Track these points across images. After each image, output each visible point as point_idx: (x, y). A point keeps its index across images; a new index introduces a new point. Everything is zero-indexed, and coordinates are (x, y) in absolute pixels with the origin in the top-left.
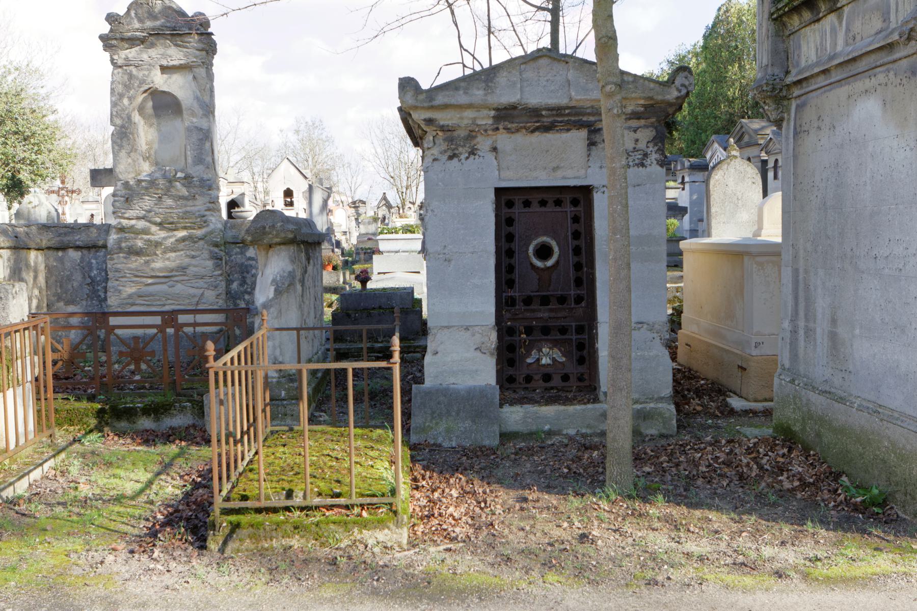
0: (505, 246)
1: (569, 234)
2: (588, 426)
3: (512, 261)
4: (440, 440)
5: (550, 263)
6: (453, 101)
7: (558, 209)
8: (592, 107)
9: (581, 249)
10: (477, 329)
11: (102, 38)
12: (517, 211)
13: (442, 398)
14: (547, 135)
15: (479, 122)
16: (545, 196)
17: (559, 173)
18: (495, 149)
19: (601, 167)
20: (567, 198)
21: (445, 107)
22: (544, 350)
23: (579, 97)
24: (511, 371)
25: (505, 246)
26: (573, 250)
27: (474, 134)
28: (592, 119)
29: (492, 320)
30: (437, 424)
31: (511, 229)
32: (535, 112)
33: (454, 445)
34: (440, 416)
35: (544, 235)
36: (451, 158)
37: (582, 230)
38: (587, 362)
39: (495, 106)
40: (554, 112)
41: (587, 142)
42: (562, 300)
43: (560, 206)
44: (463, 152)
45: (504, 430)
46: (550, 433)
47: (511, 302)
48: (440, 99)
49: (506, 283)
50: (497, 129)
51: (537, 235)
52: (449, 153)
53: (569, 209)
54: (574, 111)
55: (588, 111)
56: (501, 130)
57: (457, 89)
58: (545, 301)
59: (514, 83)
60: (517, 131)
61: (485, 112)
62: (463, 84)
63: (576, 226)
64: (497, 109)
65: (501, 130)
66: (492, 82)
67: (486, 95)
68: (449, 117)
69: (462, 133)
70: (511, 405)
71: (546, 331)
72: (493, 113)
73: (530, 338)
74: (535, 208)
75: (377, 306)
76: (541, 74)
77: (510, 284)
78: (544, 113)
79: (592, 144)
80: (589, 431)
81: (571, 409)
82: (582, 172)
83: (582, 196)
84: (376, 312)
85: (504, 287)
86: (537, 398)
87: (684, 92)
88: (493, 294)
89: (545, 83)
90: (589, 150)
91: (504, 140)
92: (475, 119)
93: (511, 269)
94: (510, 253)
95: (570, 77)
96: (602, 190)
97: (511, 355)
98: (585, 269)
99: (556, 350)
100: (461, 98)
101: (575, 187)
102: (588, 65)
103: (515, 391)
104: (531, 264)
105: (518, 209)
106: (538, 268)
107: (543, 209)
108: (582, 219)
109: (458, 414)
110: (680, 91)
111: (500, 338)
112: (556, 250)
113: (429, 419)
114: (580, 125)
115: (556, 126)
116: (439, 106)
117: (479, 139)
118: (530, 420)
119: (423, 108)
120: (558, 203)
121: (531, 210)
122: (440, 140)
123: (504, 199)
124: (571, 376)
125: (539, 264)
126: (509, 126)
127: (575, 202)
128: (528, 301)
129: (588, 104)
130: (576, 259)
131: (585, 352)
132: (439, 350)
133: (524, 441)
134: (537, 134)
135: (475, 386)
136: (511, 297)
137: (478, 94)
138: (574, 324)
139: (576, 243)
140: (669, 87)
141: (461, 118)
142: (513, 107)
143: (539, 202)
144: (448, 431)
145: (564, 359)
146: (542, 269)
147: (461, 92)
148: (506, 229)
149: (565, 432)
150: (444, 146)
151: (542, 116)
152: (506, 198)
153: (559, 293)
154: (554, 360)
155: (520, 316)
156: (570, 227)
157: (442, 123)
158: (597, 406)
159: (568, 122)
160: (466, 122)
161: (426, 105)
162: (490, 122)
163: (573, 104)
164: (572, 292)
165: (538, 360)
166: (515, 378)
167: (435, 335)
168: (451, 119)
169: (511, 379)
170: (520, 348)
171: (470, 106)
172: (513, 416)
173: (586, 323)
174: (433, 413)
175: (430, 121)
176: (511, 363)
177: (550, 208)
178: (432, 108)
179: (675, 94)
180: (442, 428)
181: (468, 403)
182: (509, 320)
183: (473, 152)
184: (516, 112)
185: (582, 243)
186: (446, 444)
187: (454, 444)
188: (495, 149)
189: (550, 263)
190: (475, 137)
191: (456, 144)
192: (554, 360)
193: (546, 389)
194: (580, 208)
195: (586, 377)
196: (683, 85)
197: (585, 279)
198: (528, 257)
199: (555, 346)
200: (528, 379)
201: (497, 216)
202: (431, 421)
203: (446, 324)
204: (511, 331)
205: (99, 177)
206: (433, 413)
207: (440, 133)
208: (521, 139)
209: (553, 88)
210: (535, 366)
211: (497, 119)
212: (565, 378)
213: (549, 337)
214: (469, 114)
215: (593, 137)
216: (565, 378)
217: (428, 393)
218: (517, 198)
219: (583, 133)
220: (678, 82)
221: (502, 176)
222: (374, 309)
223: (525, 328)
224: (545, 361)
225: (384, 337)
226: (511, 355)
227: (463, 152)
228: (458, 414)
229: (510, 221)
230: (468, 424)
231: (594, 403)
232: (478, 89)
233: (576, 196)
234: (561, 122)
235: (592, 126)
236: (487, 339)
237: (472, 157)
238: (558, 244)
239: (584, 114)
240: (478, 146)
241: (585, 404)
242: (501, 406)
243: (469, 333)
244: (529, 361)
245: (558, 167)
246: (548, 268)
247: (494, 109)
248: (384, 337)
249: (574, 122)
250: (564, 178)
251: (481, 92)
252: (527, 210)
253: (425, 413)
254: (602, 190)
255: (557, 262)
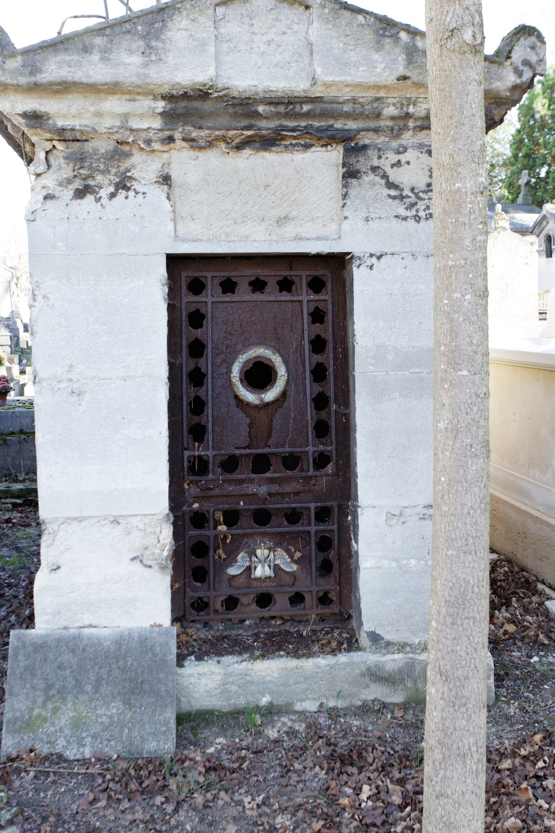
0: (187, 364)
1: (306, 343)
2: (339, 695)
3: (201, 393)
5: (270, 395)
6: (79, 76)
7: (285, 296)
8: (354, 101)
9: (325, 370)
10: (134, 521)
12: (210, 300)
13: (66, 657)
14: (267, 155)
15: (135, 124)
16: (262, 272)
17: (290, 230)
18: (166, 180)
19: (367, 220)
20: (302, 275)
21: (64, 88)
22: (259, 552)
23: (329, 79)
24: (198, 591)
25: (187, 364)
27: (126, 148)
28: (352, 125)
29: (163, 504)
30: (55, 710)
31: (198, 333)
32: (243, 107)
33: (87, 755)
34: (63, 693)
35: (260, 343)
36: (80, 194)
37: (329, 336)
38: (335, 572)
39: (165, 90)
40: (281, 109)
41: (342, 171)
42: (291, 462)
43: (289, 291)
44: (105, 183)
45: (185, 707)
46: (270, 712)
47: (200, 467)
48: (54, 70)
49: (190, 432)
50: (171, 139)
51: (247, 345)
52: (78, 184)
53: (306, 296)
54: (318, 107)
55: (346, 108)
56: (179, 143)
57: (86, 50)
58: (261, 464)
59: (204, 44)
60: (210, 144)
61: (146, 103)
62: (98, 41)
63: (317, 328)
64: (169, 98)
65: (179, 143)
66: (157, 38)
67: (145, 65)
68: (73, 111)
69: (103, 146)
70: (199, 658)
71: (262, 517)
72: (161, 105)
73: (234, 532)
74: (244, 293)
75: (17, 429)
76: (256, 29)
77: (198, 433)
78: (261, 109)
79: (351, 174)
80: (340, 704)
81: (309, 664)
82: (333, 227)
83: (329, 273)
84: (13, 438)
85: (187, 438)
86: (244, 634)
87: (527, 75)
88: (165, 456)
89: (264, 48)
90: (345, 186)
91: (184, 162)
92: (126, 117)
93: (198, 406)
94: (197, 378)
95: (312, 38)
96: (369, 262)
97: (199, 562)
98: (334, 407)
99: (280, 552)
100: (94, 70)
101: (318, 257)
102: (347, 14)
103: (206, 624)
104: (236, 397)
105: (211, 296)
106: (248, 404)
107: (258, 296)
108: (330, 316)
109: (96, 689)
110: (519, 74)
111: (177, 536)
112: (282, 371)
113: (40, 700)
114: (329, 138)
115: (284, 138)
116: (51, 84)
117: (137, 158)
118: (234, 688)
119: (18, 88)
120: (286, 285)
121: (235, 298)
122: (57, 160)
123: (186, 275)
124: (307, 596)
125: (249, 396)
126: (194, 135)
127: (316, 285)
128: (230, 464)
129: (347, 94)
130: (318, 388)
131: (332, 554)
132: (61, 562)
133: (223, 732)
134: (247, 152)
136: (200, 457)
137: (128, 63)
138: (312, 506)
139: (318, 358)
140: (500, 64)
141: (99, 114)
142: (202, 94)
143: (251, 284)
144: (77, 724)
145: (295, 567)
146: (256, 406)
147: (95, 57)
148: (188, 334)
149: (298, 707)
150: (67, 172)
151: (257, 115)
152: (190, 276)
153: (287, 449)
154: (277, 569)
155: (217, 492)
156: (308, 330)
157: (60, 123)
158: (356, 656)
159: (307, 131)
160: (108, 122)
161: (23, 80)
162: (157, 123)
163: (317, 92)
164: (310, 449)
165: (249, 570)
166: (205, 601)
167: (55, 533)
168: (79, 115)
169: (201, 605)
170: (216, 548)
171: (113, 88)
172: (203, 681)
173: (334, 504)
174: (49, 687)
175: (35, 118)
176: (200, 575)
177: (271, 294)
178: (35, 88)
179: (511, 79)
180: (64, 718)
181: (116, 666)
182: (197, 499)
183: (123, 184)
184: (207, 106)
185: (328, 358)
186: (70, 754)
187: (87, 752)
188: (166, 180)
189: (270, 395)
190: (128, 155)
191: (90, 168)
192: (277, 569)
193: (262, 619)
194: (326, 296)
195: (333, 596)
196: (526, 63)
197: (333, 425)
198: (230, 384)
199: (279, 544)
200: (231, 603)
201: (171, 308)
202: (44, 703)
203: (76, 515)
204: (199, 520)
206: (49, 687)
207: (60, 146)
208: (216, 160)
209: (279, 58)
211: (170, 117)
212: (297, 599)
214: (114, 105)
215: (353, 160)
216: (297, 599)
217: (41, 647)
218: (209, 275)
219: (335, 154)
220: (517, 55)
221: (180, 233)
222: (12, 433)
223: (226, 514)
224: (261, 571)
225: (27, 474)
226: (199, 562)
227: (105, 183)
228: (96, 689)
229: (197, 319)
230: (115, 708)
231: (349, 650)
232: (131, 52)
233: (320, 272)
234: (293, 130)
235: (350, 139)
236: (153, 540)
237: (122, 193)
238: (286, 361)
239: (338, 115)
240: (134, 173)
241: (333, 652)
242: (181, 660)
243: (119, 529)
244: (232, 571)
245: (286, 217)
246: (268, 405)
247: (164, 98)
248: (27, 474)
249: (319, 130)
250: (299, 238)
251: (136, 59)
252: (228, 297)
254: (369, 262)
255: (284, 394)
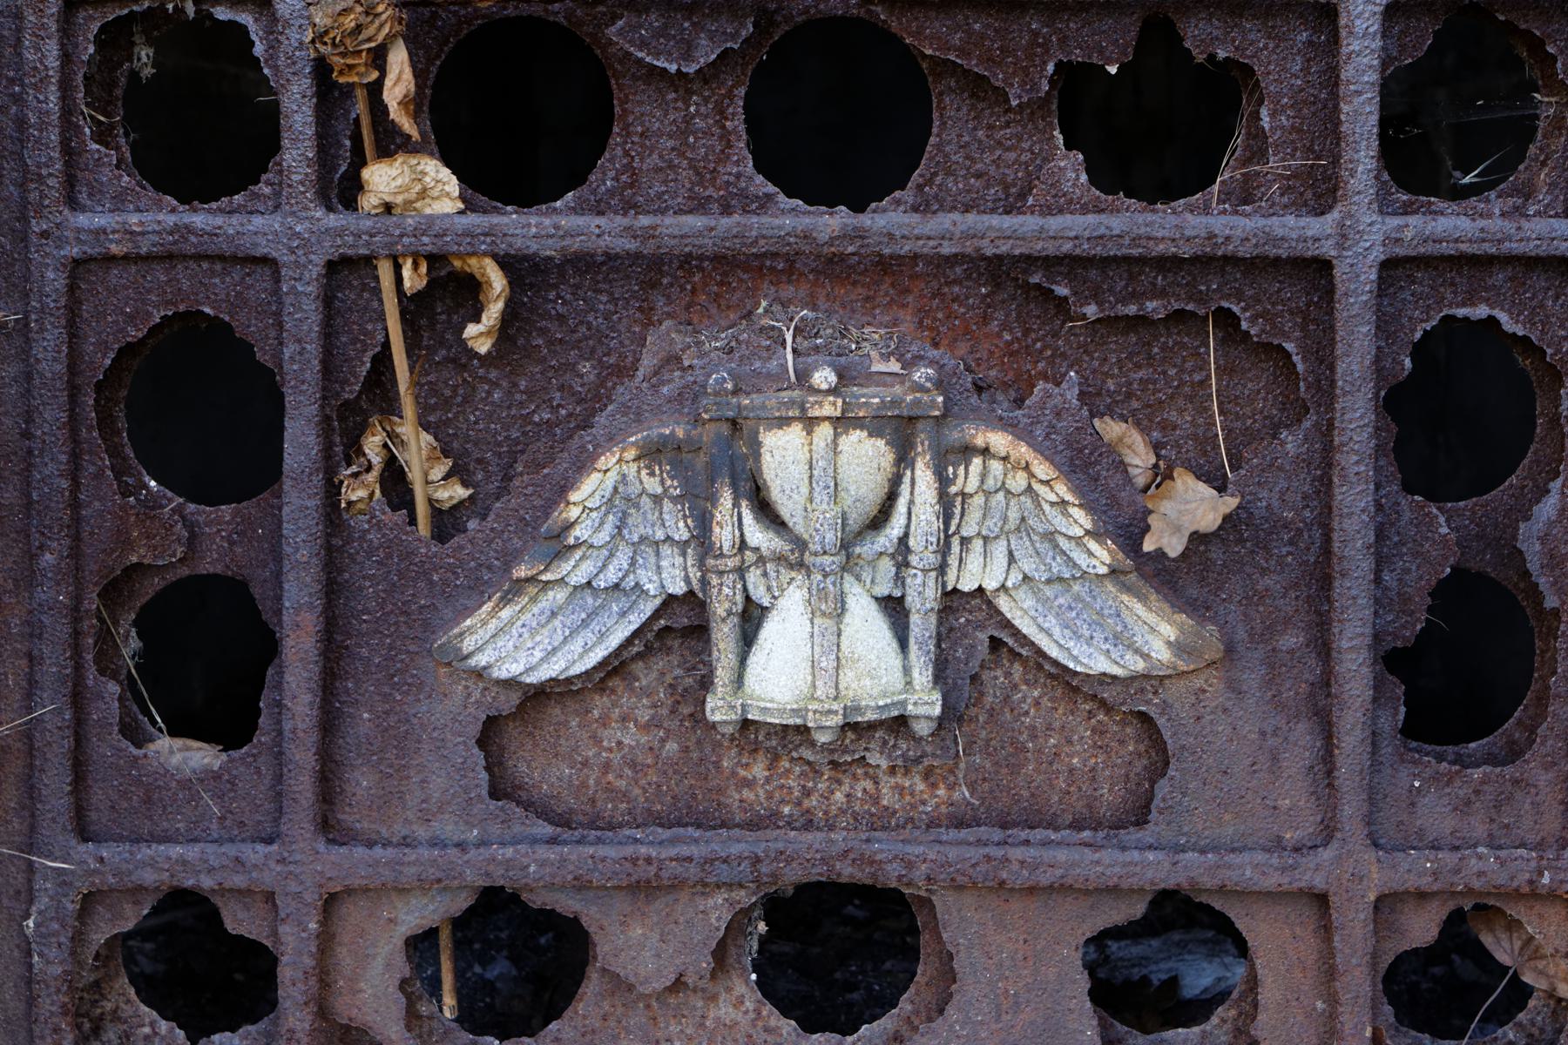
22: (784, 455)
26: (1396, 402)
73: (537, 228)
99: (1008, 465)
154: (969, 638)
170: (359, 404)
192: (969, 638)
199: (1001, 389)
210: (626, 731)
213: (891, 221)
224: (812, 658)
244: (520, 641)
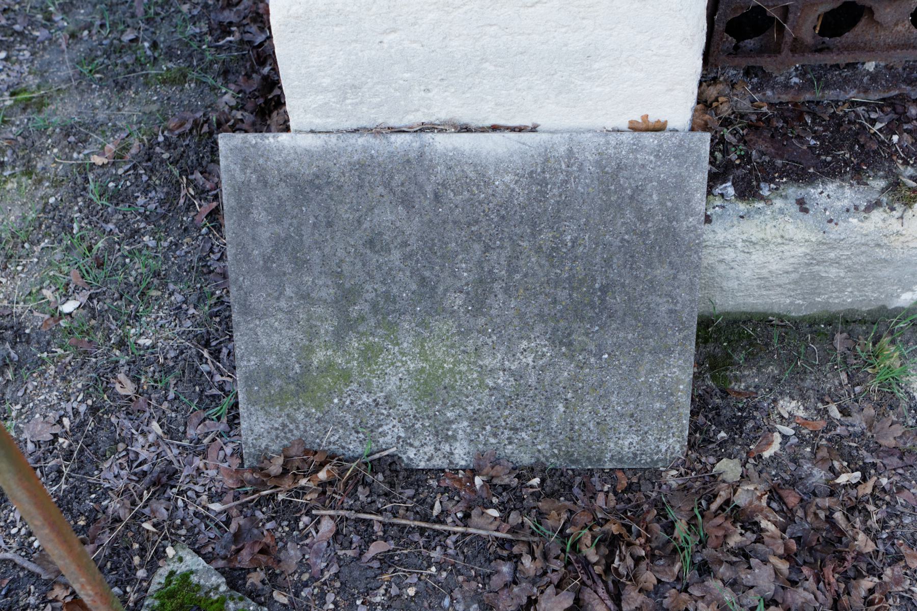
4: (390, 436)
11: (647, 116)
13: (388, 216)
30: (369, 355)
34: (386, 311)
113: (326, 328)
135: (573, 132)
144: (430, 389)
172: (757, 256)
174: (348, 296)
180: (397, 373)
186: (418, 456)
202: (339, 339)
205: (454, 437)
206: (348, 296)
217: (310, 186)
230: (531, 353)
253: (305, 297)
